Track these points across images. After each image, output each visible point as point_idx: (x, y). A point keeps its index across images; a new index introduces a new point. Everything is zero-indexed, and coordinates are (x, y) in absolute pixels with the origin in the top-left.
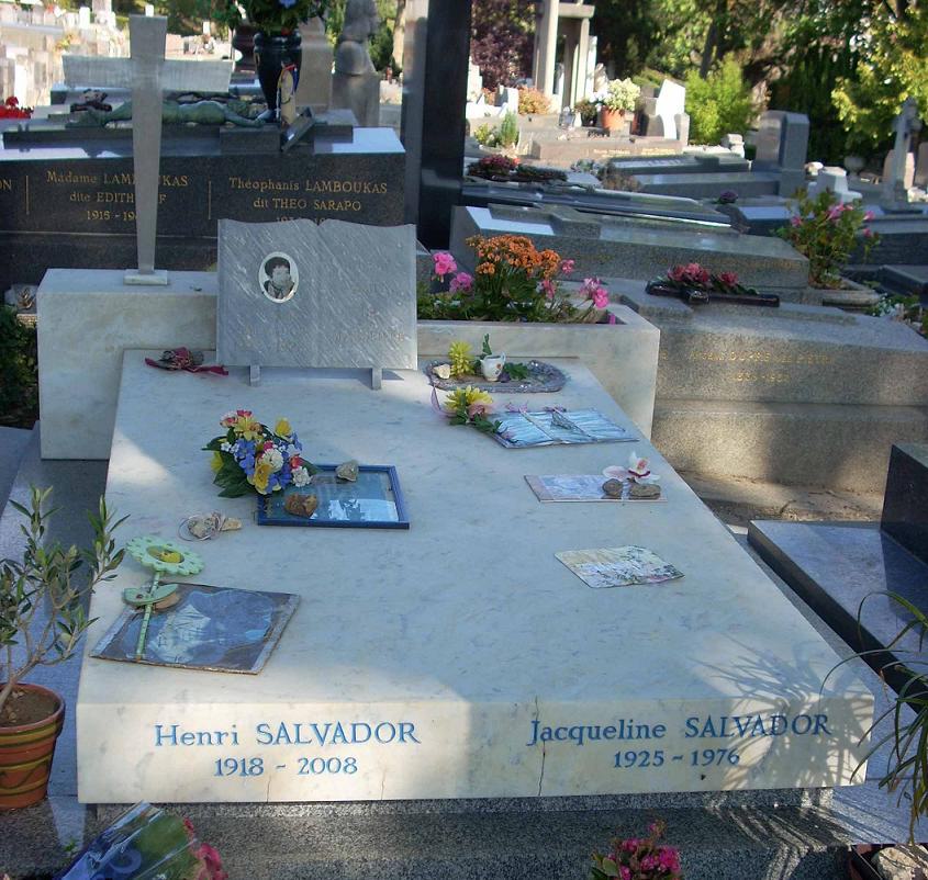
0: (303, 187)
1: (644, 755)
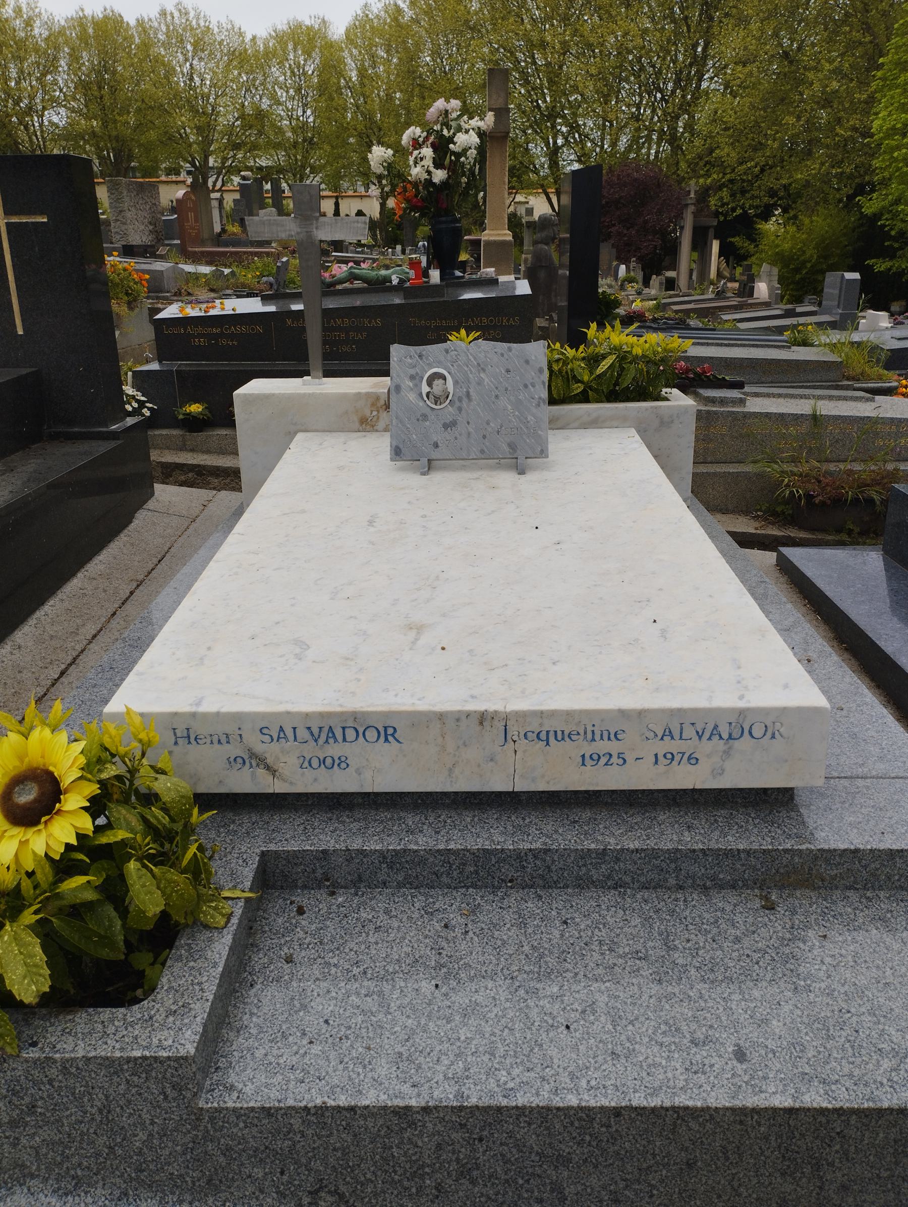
1: (608, 757)
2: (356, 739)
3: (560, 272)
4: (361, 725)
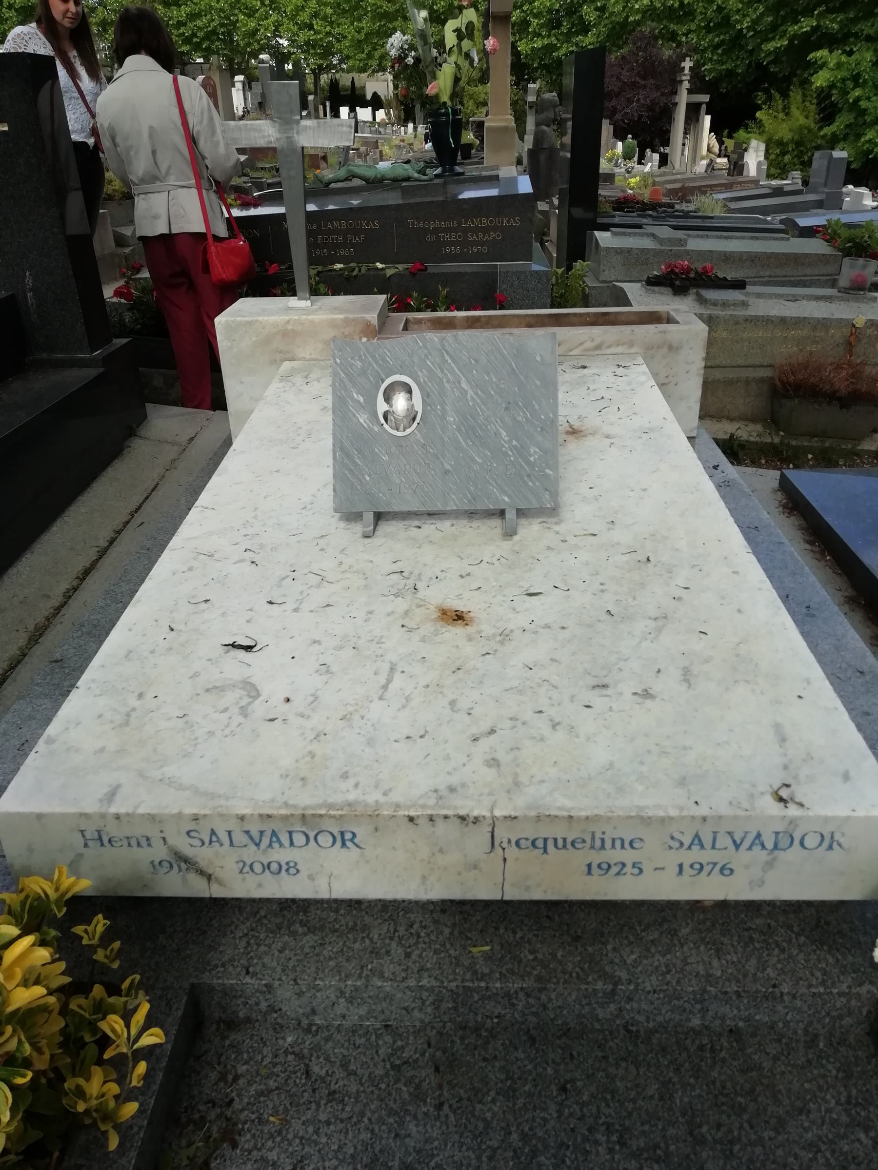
0: (460, 224)
1: (621, 866)
2: (307, 843)
3: (562, 154)
4: (312, 830)
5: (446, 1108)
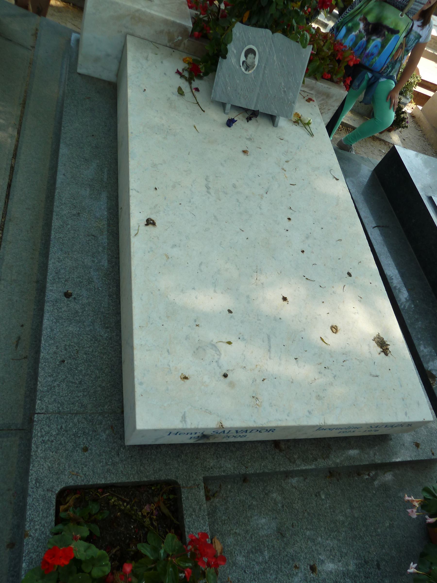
5: (285, 507)
